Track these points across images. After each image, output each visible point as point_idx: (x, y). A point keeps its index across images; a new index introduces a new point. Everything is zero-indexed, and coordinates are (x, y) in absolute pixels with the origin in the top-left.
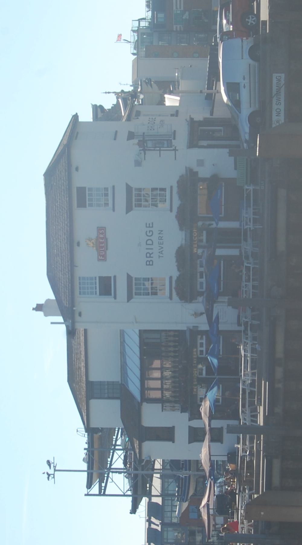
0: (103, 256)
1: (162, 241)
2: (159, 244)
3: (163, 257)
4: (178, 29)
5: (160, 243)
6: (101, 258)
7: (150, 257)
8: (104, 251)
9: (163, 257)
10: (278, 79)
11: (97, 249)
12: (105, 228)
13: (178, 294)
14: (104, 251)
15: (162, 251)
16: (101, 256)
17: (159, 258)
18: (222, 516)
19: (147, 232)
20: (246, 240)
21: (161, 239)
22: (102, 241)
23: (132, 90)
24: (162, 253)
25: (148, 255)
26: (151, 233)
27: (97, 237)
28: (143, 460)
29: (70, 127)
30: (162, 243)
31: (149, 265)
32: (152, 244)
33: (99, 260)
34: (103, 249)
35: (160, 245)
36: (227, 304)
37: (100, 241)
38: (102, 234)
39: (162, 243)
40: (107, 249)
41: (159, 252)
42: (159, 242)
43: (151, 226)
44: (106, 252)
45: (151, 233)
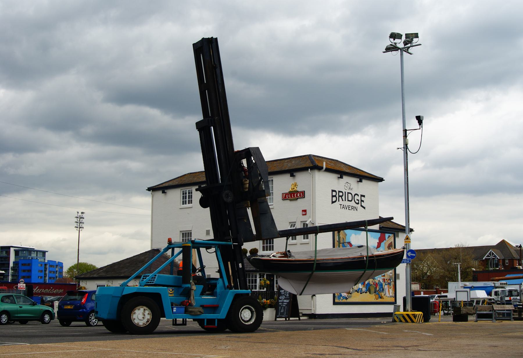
0: (285, 197)
1: (350, 209)
2: (349, 206)
3: (341, 208)
4: (42, 259)
5: (349, 207)
6: (284, 196)
7: (339, 196)
8: (289, 197)
9: (341, 208)
10: (520, 293)
11: (290, 192)
12: (304, 197)
13: (27, 323)
14: (289, 197)
15: (344, 208)
16: (286, 195)
17: (340, 204)
18: (192, 250)
19: (358, 195)
20: (446, 296)
21: (352, 208)
22: (295, 195)
23: (243, 245)
24: (343, 207)
25: (353, 207)
26: (357, 202)
27: (298, 191)
28: (441, 311)
29: (373, 177)
30: (349, 209)
31: (333, 196)
32: (348, 201)
33: (283, 194)
34: (290, 197)
35: (348, 206)
36: (452, 319)
37: (295, 194)
38: (300, 195)
39: (349, 209)
40: (291, 200)
41: (343, 205)
42: (350, 206)
43: (363, 204)
44: (288, 199)
45: (357, 202)
